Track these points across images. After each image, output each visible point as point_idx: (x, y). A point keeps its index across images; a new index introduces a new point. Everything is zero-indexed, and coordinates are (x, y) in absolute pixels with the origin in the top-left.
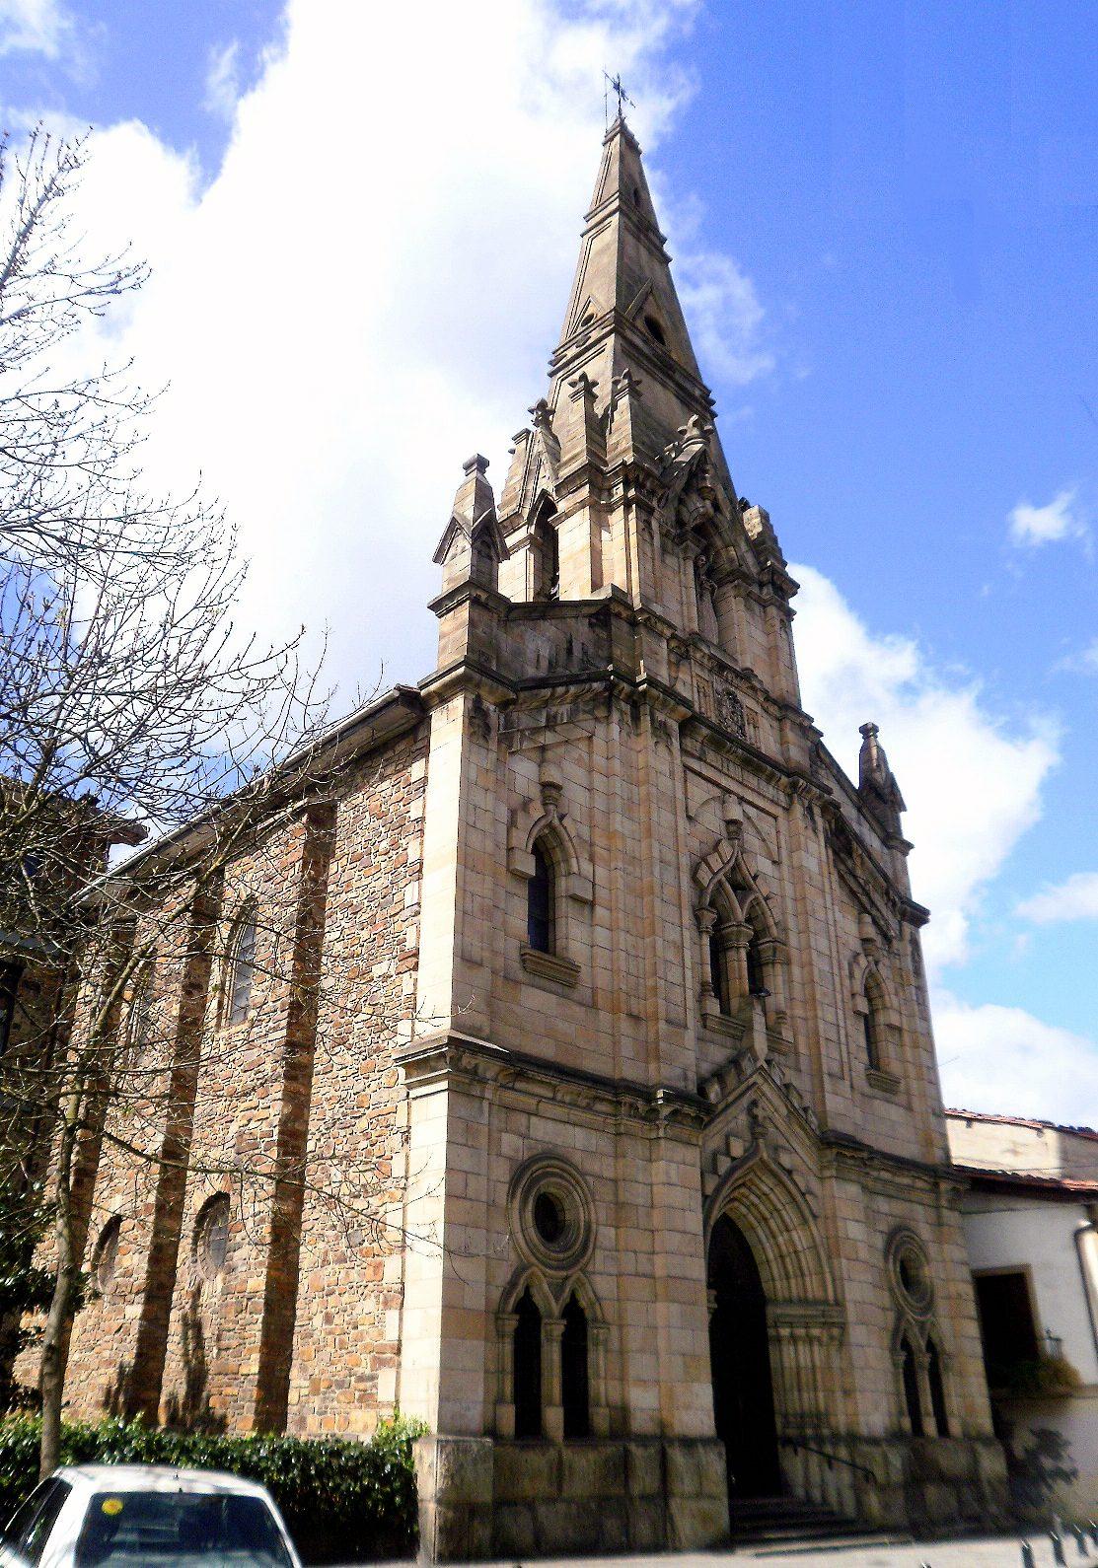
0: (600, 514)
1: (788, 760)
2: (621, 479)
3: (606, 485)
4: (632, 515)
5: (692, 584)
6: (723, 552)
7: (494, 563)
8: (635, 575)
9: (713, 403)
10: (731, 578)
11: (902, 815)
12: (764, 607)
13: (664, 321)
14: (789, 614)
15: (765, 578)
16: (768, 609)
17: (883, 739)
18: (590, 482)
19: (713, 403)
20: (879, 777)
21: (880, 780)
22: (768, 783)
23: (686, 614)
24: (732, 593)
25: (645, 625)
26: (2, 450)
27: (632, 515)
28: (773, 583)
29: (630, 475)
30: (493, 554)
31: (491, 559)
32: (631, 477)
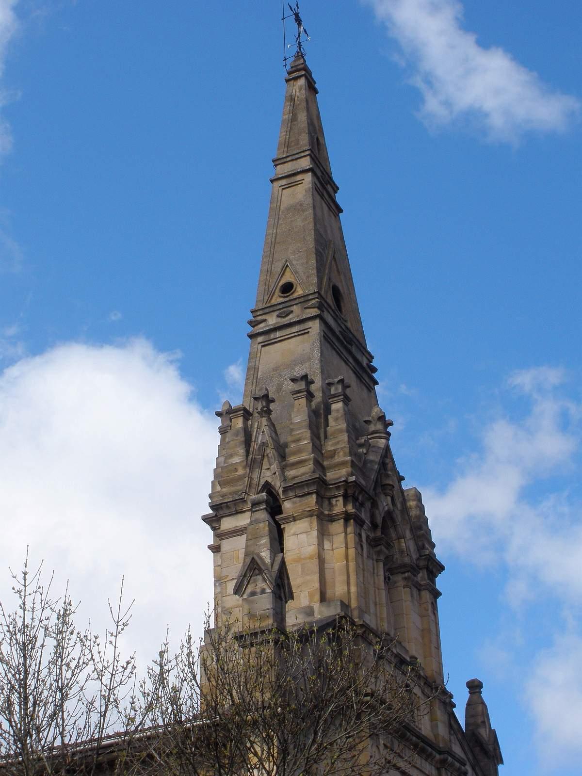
0: (324, 520)
1: (436, 736)
2: (342, 492)
3: (328, 494)
4: (350, 529)
5: (382, 585)
6: (396, 542)
7: (284, 602)
8: (353, 589)
9: (374, 370)
10: (402, 570)
11: (500, 767)
12: (419, 590)
13: (342, 289)
14: (436, 594)
15: (422, 563)
16: (423, 593)
17: (485, 694)
18: (318, 494)
19: (374, 370)
20: (483, 733)
21: (485, 736)
22: (426, 760)
23: (378, 615)
24: (401, 583)
25: (362, 637)
26: (1, 735)
27: (350, 529)
28: (427, 568)
29: (351, 492)
30: (283, 595)
31: (281, 600)
32: (350, 492)
